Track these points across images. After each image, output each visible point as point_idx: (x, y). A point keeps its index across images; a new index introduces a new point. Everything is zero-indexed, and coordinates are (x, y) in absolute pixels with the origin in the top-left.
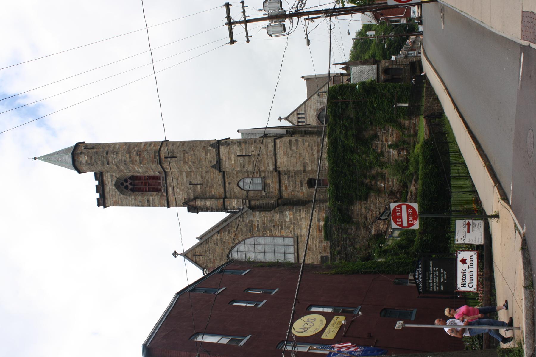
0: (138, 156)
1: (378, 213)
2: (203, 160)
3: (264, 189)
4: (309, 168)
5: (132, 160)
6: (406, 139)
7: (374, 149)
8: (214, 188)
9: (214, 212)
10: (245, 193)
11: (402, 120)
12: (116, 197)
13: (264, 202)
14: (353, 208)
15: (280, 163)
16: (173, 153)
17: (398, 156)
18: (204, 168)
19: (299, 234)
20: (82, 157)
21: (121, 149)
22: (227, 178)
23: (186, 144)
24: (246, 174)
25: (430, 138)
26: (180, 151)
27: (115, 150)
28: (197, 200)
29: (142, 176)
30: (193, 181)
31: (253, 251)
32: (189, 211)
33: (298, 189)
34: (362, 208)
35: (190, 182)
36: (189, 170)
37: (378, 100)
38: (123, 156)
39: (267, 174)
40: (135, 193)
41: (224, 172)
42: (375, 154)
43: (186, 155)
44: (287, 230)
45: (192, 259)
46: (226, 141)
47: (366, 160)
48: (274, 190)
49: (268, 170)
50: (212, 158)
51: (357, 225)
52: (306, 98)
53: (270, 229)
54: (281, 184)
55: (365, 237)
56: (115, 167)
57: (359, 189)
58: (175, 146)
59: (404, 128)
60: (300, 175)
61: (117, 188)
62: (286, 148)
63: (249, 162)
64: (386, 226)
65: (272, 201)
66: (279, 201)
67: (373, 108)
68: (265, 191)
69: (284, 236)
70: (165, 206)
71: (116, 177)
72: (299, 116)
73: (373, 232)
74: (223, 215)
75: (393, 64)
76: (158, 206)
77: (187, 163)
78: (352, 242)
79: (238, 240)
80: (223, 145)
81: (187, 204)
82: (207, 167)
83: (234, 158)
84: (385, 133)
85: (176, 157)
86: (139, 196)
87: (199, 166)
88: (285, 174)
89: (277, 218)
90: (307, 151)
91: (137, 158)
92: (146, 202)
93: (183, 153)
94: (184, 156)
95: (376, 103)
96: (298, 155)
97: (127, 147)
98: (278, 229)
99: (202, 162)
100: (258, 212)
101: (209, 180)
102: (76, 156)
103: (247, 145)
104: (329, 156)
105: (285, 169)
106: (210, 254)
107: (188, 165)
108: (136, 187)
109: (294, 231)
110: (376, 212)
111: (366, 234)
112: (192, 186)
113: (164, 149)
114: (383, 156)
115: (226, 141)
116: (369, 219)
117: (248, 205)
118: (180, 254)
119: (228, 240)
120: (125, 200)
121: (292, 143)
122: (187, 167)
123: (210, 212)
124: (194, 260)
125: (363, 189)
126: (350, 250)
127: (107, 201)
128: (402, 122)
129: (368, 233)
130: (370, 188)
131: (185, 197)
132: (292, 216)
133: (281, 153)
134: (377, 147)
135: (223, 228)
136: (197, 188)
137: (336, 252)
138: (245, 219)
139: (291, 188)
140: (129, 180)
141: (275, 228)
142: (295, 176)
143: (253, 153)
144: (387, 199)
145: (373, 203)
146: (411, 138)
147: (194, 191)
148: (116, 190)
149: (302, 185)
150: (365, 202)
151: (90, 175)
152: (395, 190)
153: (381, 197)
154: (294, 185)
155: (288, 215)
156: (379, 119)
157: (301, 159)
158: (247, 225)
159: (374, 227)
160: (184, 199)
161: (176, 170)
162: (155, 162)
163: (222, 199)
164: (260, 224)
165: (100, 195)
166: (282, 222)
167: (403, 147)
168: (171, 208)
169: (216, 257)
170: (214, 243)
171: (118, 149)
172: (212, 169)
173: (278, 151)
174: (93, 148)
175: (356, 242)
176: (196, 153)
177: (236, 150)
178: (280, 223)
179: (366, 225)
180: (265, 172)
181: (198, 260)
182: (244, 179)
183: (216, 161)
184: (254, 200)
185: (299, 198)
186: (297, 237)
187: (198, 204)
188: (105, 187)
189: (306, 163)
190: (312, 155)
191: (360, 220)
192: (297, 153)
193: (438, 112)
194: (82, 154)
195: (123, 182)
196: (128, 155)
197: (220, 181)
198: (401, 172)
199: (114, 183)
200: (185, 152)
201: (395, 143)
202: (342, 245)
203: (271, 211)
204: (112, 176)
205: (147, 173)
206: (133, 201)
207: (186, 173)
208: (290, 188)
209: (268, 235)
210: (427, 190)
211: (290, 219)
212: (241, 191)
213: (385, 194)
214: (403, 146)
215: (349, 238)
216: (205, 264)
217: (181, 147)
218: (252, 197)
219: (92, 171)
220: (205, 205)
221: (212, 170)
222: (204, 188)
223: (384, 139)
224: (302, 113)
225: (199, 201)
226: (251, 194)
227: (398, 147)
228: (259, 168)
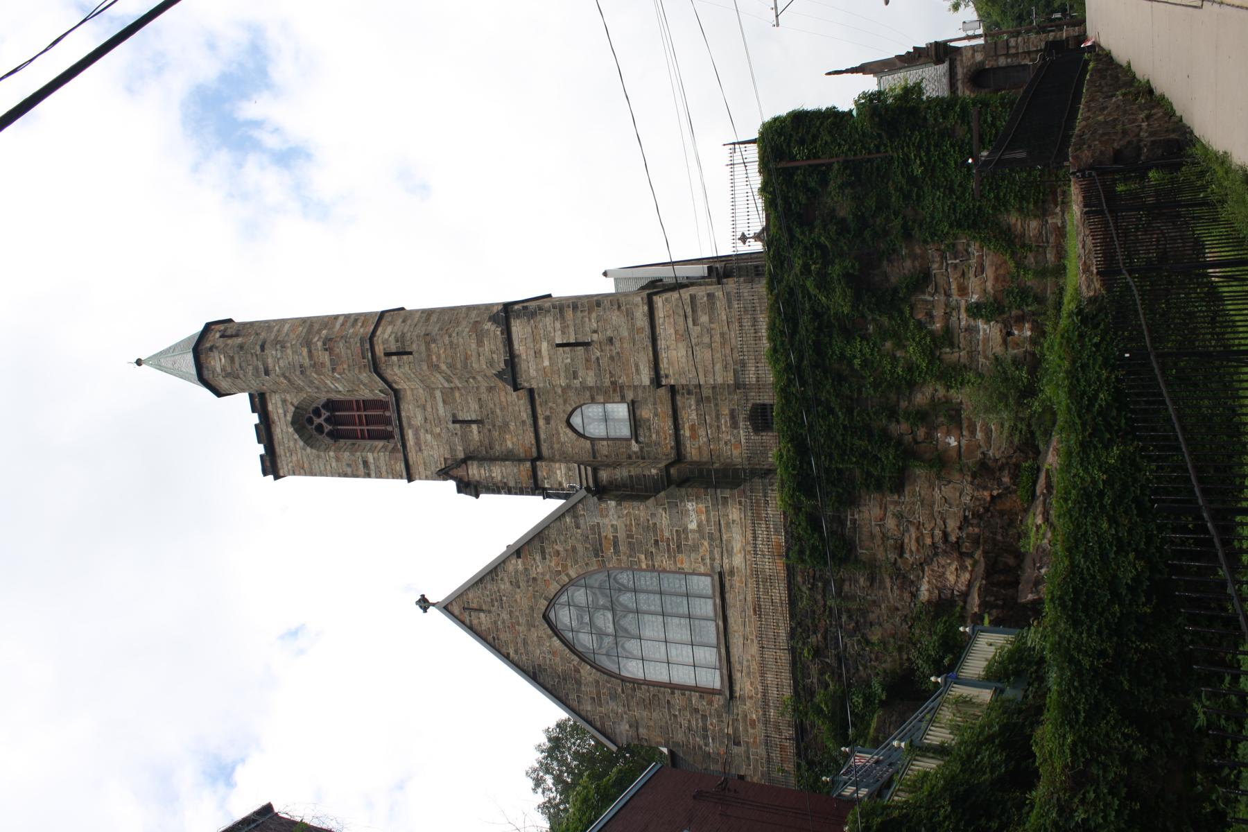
0: (328, 352)
1: (937, 532)
2: (474, 359)
3: (635, 434)
5: (315, 363)
6: (1029, 284)
7: (919, 321)
8: (510, 432)
9: (516, 494)
11: (1014, 219)
13: (632, 473)
14: (856, 516)
15: (668, 363)
16: (403, 343)
17: (1005, 342)
18: (479, 378)
21: (292, 336)
22: (541, 405)
23: (434, 318)
24: (588, 394)
25: (1109, 290)
26: (418, 336)
27: (279, 338)
28: (469, 462)
29: (351, 402)
30: (460, 413)
34: (885, 515)
35: (454, 415)
36: (446, 385)
37: (928, 152)
38: (296, 352)
39: (640, 392)
40: (337, 444)
41: (531, 392)
42: (925, 337)
43: (433, 345)
45: (463, 619)
46: (525, 304)
47: (894, 357)
48: (663, 437)
50: (494, 353)
51: (873, 570)
53: (647, 550)
54: (681, 422)
55: (897, 609)
57: (875, 456)
58: (409, 322)
59: (1023, 246)
61: (297, 431)
63: (588, 360)
64: (967, 576)
65: (654, 471)
66: (672, 471)
67: (912, 180)
68: (637, 441)
69: (686, 570)
71: (293, 405)
73: (924, 592)
74: (536, 509)
75: (997, 56)
76: (388, 478)
77: (437, 367)
78: (857, 623)
79: (567, 575)
80: (518, 317)
82: (485, 375)
83: (548, 351)
84: (955, 266)
85: (411, 353)
86: (344, 452)
88: (689, 393)
89: (664, 519)
91: (325, 358)
93: (425, 342)
94: (428, 349)
95: (922, 164)
96: (717, 338)
97: (305, 330)
98: (669, 550)
99: (471, 363)
100: (613, 503)
102: (203, 357)
103: (579, 314)
104: (774, 350)
106: (502, 608)
110: (933, 529)
111: (902, 599)
112: (458, 426)
114: (952, 345)
115: (525, 304)
116: (911, 551)
119: (542, 574)
120: (316, 461)
121: (699, 305)
123: (506, 493)
124: (468, 622)
125: (887, 457)
126: (853, 645)
128: (1015, 225)
129: (906, 595)
130: (908, 454)
132: (703, 517)
133: (670, 335)
134: (930, 315)
136: (471, 431)
137: (809, 651)
138: (582, 521)
141: (661, 549)
143: (595, 337)
144: (969, 489)
145: (922, 501)
146: (1050, 281)
147: (464, 438)
148: (296, 436)
150: (896, 497)
151: (241, 400)
152: (996, 460)
153: (949, 482)
155: (694, 513)
156: (933, 218)
158: (588, 537)
159: (926, 580)
160: (442, 459)
162: (365, 366)
163: (528, 460)
164: (621, 535)
166: (677, 531)
167: (1020, 312)
168: (417, 483)
171: (287, 334)
173: (660, 330)
175: (871, 624)
176: (455, 341)
178: (672, 534)
179: (900, 570)
181: (475, 622)
182: (583, 407)
183: (505, 360)
184: (608, 466)
185: (729, 461)
186: (721, 575)
187: (474, 475)
188: (273, 430)
191: (880, 555)
192: (713, 332)
193: (1153, 143)
194: (214, 350)
195: (312, 415)
197: (525, 415)
198: (1011, 401)
199: (289, 418)
200: (428, 338)
201: (991, 299)
202: (826, 631)
204: (284, 401)
205: (355, 393)
207: (441, 392)
209: (644, 566)
210: (1094, 577)
212: (577, 440)
213: (961, 470)
214: (1019, 307)
215: (848, 611)
218: (606, 456)
219: (243, 390)
222: (486, 431)
223: (954, 286)
225: (475, 466)
226: (603, 448)
227: (1002, 312)
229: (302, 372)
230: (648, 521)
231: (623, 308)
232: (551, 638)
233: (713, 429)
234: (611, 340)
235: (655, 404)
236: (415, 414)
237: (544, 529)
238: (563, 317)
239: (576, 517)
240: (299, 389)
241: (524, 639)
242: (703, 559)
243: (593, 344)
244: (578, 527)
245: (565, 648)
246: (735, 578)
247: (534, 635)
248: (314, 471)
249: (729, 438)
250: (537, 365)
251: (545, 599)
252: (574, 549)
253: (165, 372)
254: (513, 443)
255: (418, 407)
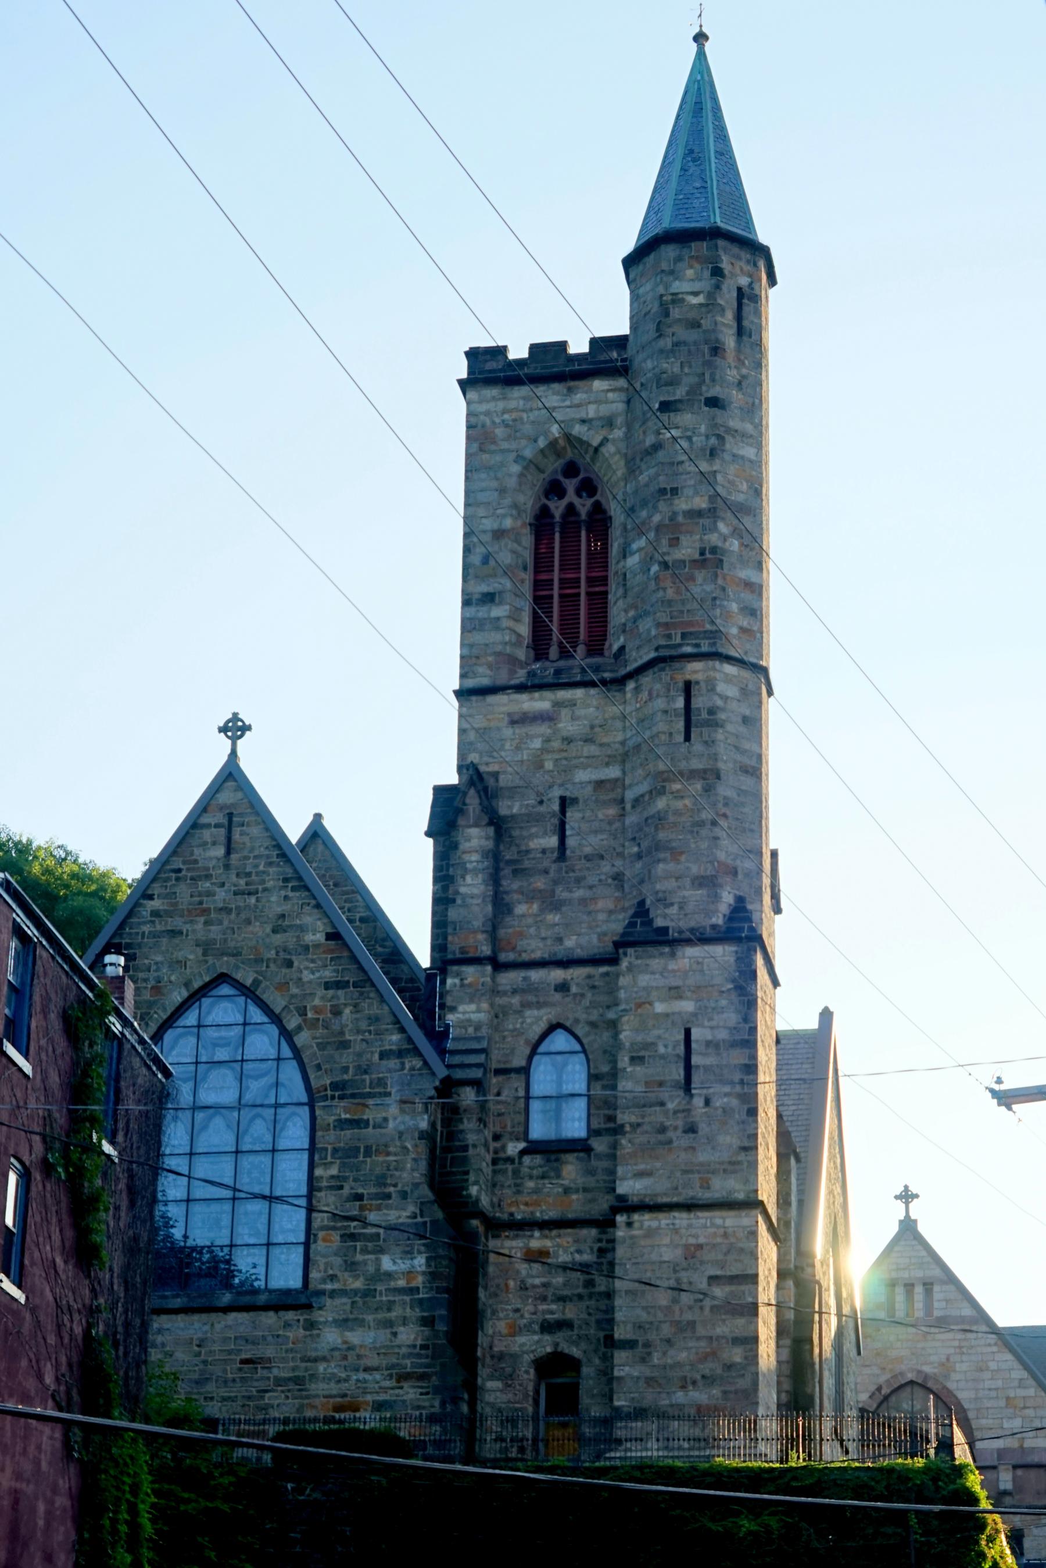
0: (697, 556)
3: (534, 1148)
4: (624, 1365)
8: (542, 910)
10: (519, 1062)
12: (508, 438)
18: (639, 865)
19: (320, 1316)
20: (699, 278)
21: (732, 469)
22: (589, 977)
23: (747, 782)
24: (605, 1068)
27: (729, 439)
28: (491, 830)
29: (605, 567)
30: (579, 815)
31: (248, 1098)
32: (440, 792)
33: (531, 1308)
35: (575, 801)
36: (630, 795)
40: (527, 530)
41: (613, 961)
43: (699, 786)
44: (338, 1261)
49: (620, 1171)
50: (681, 908)
52: (1002, 1320)
54: (554, 1232)
56: (650, 440)
58: (742, 729)
60: (598, 1322)
62: (720, 1257)
68: (523, 1153)
69: (313, 1246)
70: (463, 676)
72: (919, 1290)
76: (463, 645)
79: (299, 1028)
81: (471, 783)
82: (642, 882)
83: (679, 1013)
85: (687, 738)
86: (513, 552)
87: (645, 844)
88: (601, 1252)
90: (704, 1358)
91: (687, 549)
92: (484, 588)
93: (705, 771)
96: (688, 1316)
101: (579, 893)
103: (737, 1076)
105: (621, 1252)
106: (235, 894)
107: (651, 792)
108: (557, 536)
109: (333, 1294)
112: (556, 807)
113: (728, 679)
117: (459, 1074)
118: (233, 753)
120: (494, 484)
121: (743, 1288)
122: (643, 788)
124: (205, 819)
127: (494, 399)
131: (505, 772)
132: (401, 1283)
135: (354, 959)
136: (545, 833)
138: (393, 1063)
139: (534, 1275)
140: (589, 502)
141: (348, 1205)
142: (591, 1296)
148: (542, 443)
149: (548, 1327)
154: (551, 1291)
157: (666, 1330)
158: (366, 1072)
161: (629, 734)
163: (494, 951)
165: (520, 363)
166: (378, 1235)
169: (220, 923)
170: (283, 916)
172: (630, 903)
174: (740, 332)
177: (714, 1023)
180: (613, 1157)
181: (207, 835)
182: (582, 1056)
189: (649, 1354)
190: (685, 1378)
195: (581, 476)
196: (704, 505)
199: (578, 430)
203: (426, 1187)
204: (609, 422)
205: (621, 591)
206: (489, 524)
207: (616, 780)
208: (534, 1272)
211: (389, 1275)
212: (527, 1042)
216: (188, 870)
217: (735, 761)
219: (634, 327)
220: (466, 871)
221: (627, 904)
222: (546, 863)
224: (936, 1305)
225: (484, 842)
228: (628, 1128)
229: (663, 491)
230: (395, 1185)
231: (742, 1157)
232: (187, 985)
233: (541, 1290)
234: (691, 1129)
235: (585, 1190)
236: (578, 718)
237: (378, 991)
238: (734, 1044)
239: (400, 1054)
240: (632, 470)
241: (181, 933)
242: (333, 1278)
243: (687, 1098)
244: (383, 1055)
245: (169, 1013)
246: (301, 1331)
247: (191, 954)
248: (475, 476)
249: (527, 1315)
250: (657, 988)
251: (256, 983)
252: (344, 1045)
253: (678, 116)
254: (523, 916)
255: (592, 727)
